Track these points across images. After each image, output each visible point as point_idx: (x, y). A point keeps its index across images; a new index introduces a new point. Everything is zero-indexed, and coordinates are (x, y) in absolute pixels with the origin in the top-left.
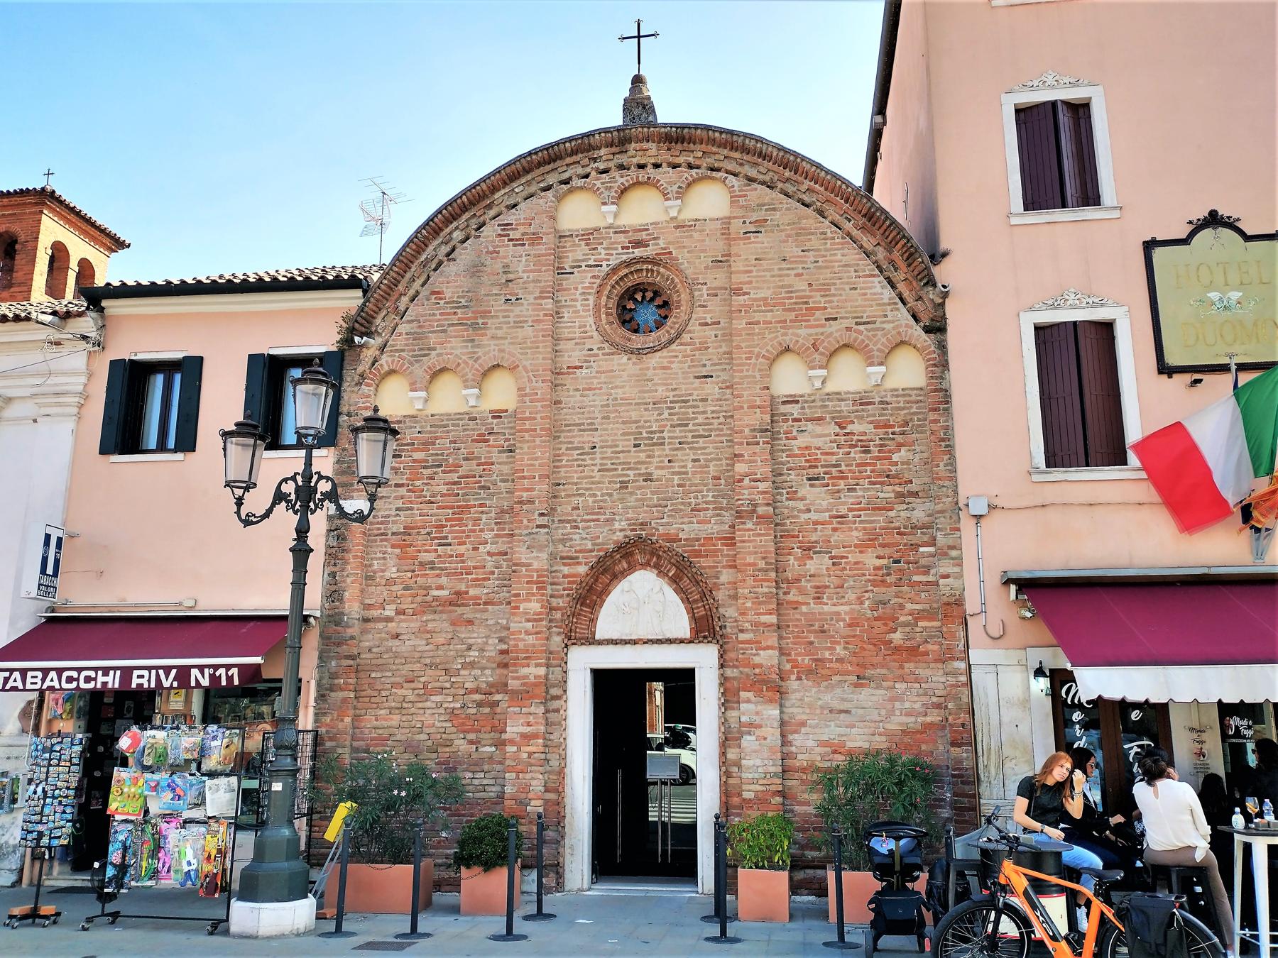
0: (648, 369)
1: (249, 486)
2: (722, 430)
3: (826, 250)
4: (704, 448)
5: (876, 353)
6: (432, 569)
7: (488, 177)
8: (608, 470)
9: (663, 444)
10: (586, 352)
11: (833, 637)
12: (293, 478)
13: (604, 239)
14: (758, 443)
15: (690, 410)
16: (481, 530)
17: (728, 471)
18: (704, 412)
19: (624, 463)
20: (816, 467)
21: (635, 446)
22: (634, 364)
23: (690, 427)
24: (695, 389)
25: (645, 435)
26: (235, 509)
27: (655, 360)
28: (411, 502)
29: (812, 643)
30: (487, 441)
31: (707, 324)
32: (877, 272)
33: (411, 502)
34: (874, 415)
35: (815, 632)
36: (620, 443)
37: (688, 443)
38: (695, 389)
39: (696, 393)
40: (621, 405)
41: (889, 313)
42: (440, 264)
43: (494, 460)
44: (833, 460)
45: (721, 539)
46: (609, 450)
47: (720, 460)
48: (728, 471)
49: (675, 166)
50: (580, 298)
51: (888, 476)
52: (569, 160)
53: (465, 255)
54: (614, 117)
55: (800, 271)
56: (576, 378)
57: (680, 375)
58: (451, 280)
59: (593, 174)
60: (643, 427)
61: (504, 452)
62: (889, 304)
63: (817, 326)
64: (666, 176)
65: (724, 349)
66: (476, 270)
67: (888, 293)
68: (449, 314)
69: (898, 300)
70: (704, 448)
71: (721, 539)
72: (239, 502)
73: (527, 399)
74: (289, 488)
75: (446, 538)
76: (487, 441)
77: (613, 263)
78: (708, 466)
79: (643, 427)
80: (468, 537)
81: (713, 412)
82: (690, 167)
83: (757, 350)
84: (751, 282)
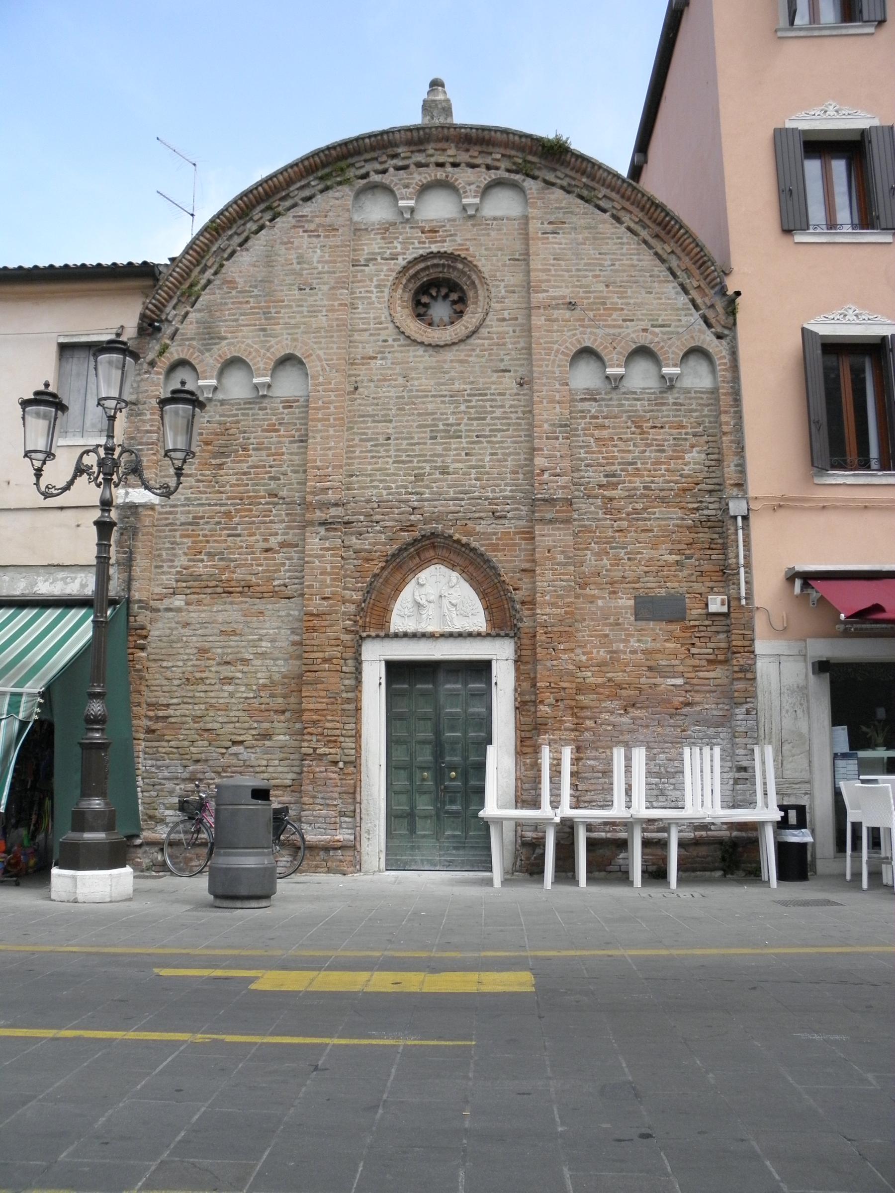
0: (445, 361)
1: (49, 455)
2: (520, 424)
3: (622, 255)
4: (502, 442)
5: (671, 356)
6: (221, 559)
7: (285, 169)
8: (403, 462)
9: (460, 437)
10: (380, 343)
11: (627, 629)
12: (95, 451)
13: (401, 234)
14: (557, 438)
15: (488, 404)
16: (271, 522)
17: (526, 465)
18: (502, 406)
19: (420, 456)
20: (613, 464)
21: (432, 438)
22: (430, 356)
23: (488, 421)
24: (493, 383)
25: (441, 427)
26: (34, 480)
27: (449, 355)
28: (200, 492)
29: (607, 636)
30: (278, 431)
31: (504, 320)
32: (671, 278)
33: (200, 492)
34: (668, 416)
35: (611, 625)
36: (416, 436)
37: (485, 436)
38: (493, 383)
39: (493, 387)
40: (417, 397)
41: (683, 318)
42: (233, 253)
43: (284, 450)
44: (629, 457)
45: (518, 533)
46: (405, 442)
47: (519, 454)
48: (526, 465)
49: (473, 166)
50: (375, 290)
51: (681, 476)
52: (368, 156)
53: (258, 244)
54: (414, 117)
55: (598, 273)
56: (371, 369)
57: (477, 369)
58: (244, 266)
59: (391, 170)
60: (440, 420)
61: (295, 442)
62: (683, 309)
63: (614, 326)
64: (463, 177)
65: (522, 344)
66: (269, 261)
67: (683, 299)
68: (240, 303)
69: (691, 306)
70: (502, 442)
71: (518, 533)
72: (38, 473)
73: (320, 388)
74: (91, 460)
75: (236, 529)
76: (278, 431)
77: (410, 257)
78: (506, 460)
79: (440, 420)
80: (258, 528)
81: (511, 406)
82: (489, 168)
83: (556, 346)
84: (548, 281)
